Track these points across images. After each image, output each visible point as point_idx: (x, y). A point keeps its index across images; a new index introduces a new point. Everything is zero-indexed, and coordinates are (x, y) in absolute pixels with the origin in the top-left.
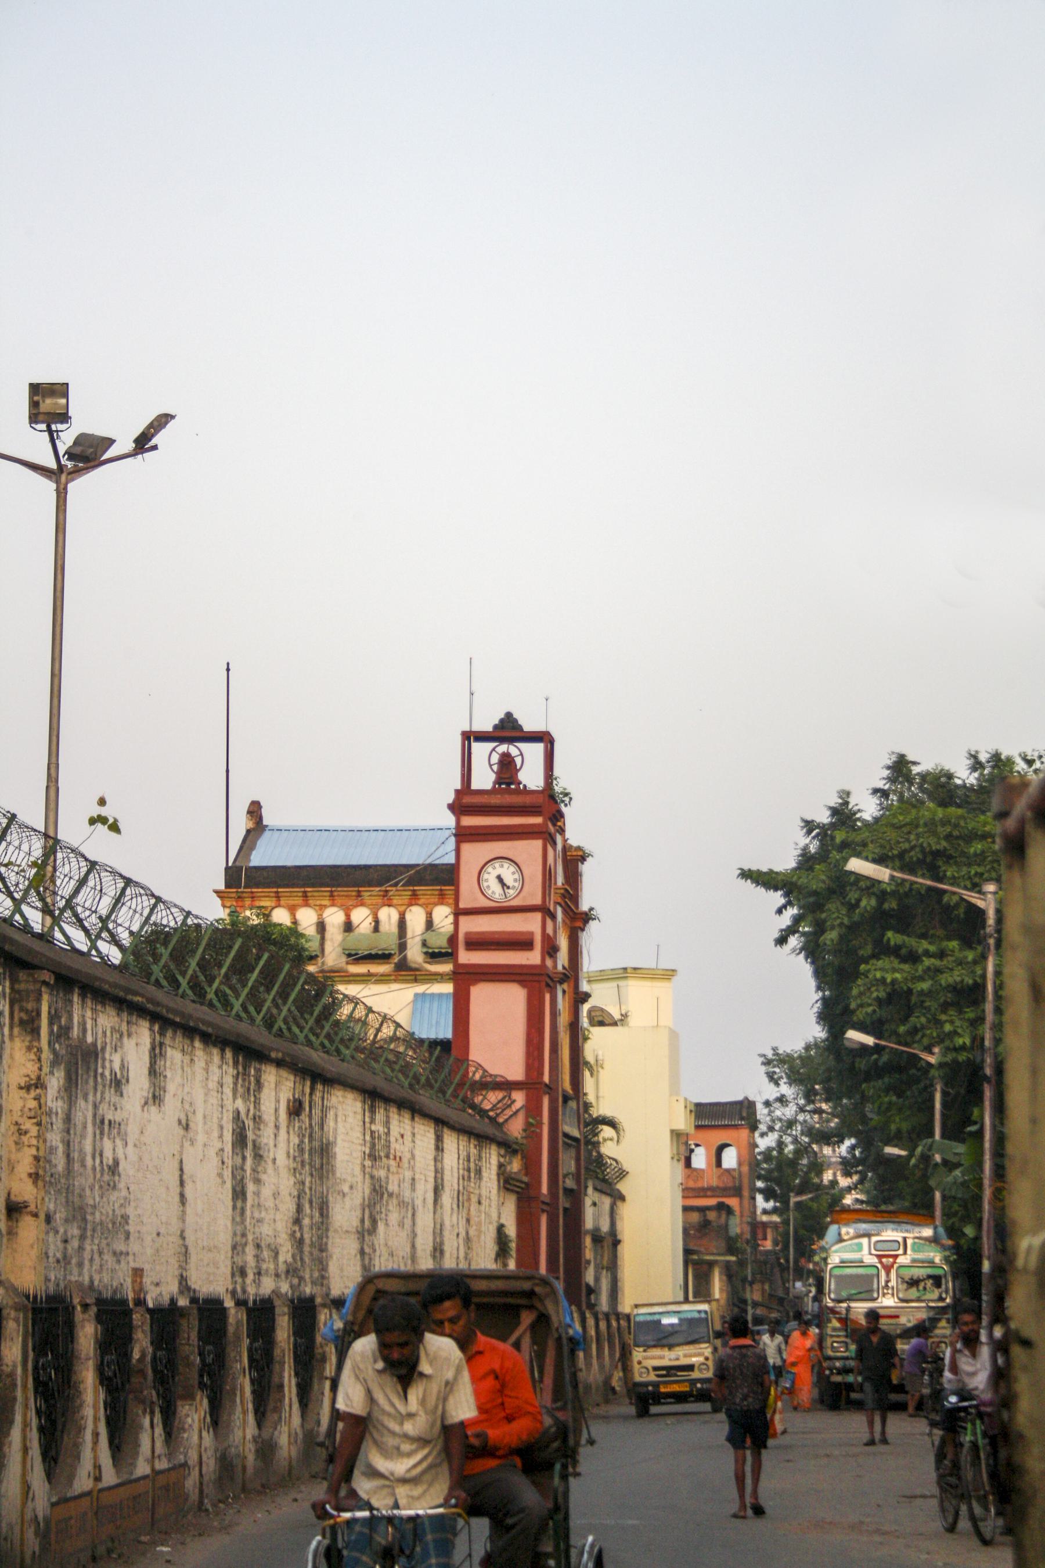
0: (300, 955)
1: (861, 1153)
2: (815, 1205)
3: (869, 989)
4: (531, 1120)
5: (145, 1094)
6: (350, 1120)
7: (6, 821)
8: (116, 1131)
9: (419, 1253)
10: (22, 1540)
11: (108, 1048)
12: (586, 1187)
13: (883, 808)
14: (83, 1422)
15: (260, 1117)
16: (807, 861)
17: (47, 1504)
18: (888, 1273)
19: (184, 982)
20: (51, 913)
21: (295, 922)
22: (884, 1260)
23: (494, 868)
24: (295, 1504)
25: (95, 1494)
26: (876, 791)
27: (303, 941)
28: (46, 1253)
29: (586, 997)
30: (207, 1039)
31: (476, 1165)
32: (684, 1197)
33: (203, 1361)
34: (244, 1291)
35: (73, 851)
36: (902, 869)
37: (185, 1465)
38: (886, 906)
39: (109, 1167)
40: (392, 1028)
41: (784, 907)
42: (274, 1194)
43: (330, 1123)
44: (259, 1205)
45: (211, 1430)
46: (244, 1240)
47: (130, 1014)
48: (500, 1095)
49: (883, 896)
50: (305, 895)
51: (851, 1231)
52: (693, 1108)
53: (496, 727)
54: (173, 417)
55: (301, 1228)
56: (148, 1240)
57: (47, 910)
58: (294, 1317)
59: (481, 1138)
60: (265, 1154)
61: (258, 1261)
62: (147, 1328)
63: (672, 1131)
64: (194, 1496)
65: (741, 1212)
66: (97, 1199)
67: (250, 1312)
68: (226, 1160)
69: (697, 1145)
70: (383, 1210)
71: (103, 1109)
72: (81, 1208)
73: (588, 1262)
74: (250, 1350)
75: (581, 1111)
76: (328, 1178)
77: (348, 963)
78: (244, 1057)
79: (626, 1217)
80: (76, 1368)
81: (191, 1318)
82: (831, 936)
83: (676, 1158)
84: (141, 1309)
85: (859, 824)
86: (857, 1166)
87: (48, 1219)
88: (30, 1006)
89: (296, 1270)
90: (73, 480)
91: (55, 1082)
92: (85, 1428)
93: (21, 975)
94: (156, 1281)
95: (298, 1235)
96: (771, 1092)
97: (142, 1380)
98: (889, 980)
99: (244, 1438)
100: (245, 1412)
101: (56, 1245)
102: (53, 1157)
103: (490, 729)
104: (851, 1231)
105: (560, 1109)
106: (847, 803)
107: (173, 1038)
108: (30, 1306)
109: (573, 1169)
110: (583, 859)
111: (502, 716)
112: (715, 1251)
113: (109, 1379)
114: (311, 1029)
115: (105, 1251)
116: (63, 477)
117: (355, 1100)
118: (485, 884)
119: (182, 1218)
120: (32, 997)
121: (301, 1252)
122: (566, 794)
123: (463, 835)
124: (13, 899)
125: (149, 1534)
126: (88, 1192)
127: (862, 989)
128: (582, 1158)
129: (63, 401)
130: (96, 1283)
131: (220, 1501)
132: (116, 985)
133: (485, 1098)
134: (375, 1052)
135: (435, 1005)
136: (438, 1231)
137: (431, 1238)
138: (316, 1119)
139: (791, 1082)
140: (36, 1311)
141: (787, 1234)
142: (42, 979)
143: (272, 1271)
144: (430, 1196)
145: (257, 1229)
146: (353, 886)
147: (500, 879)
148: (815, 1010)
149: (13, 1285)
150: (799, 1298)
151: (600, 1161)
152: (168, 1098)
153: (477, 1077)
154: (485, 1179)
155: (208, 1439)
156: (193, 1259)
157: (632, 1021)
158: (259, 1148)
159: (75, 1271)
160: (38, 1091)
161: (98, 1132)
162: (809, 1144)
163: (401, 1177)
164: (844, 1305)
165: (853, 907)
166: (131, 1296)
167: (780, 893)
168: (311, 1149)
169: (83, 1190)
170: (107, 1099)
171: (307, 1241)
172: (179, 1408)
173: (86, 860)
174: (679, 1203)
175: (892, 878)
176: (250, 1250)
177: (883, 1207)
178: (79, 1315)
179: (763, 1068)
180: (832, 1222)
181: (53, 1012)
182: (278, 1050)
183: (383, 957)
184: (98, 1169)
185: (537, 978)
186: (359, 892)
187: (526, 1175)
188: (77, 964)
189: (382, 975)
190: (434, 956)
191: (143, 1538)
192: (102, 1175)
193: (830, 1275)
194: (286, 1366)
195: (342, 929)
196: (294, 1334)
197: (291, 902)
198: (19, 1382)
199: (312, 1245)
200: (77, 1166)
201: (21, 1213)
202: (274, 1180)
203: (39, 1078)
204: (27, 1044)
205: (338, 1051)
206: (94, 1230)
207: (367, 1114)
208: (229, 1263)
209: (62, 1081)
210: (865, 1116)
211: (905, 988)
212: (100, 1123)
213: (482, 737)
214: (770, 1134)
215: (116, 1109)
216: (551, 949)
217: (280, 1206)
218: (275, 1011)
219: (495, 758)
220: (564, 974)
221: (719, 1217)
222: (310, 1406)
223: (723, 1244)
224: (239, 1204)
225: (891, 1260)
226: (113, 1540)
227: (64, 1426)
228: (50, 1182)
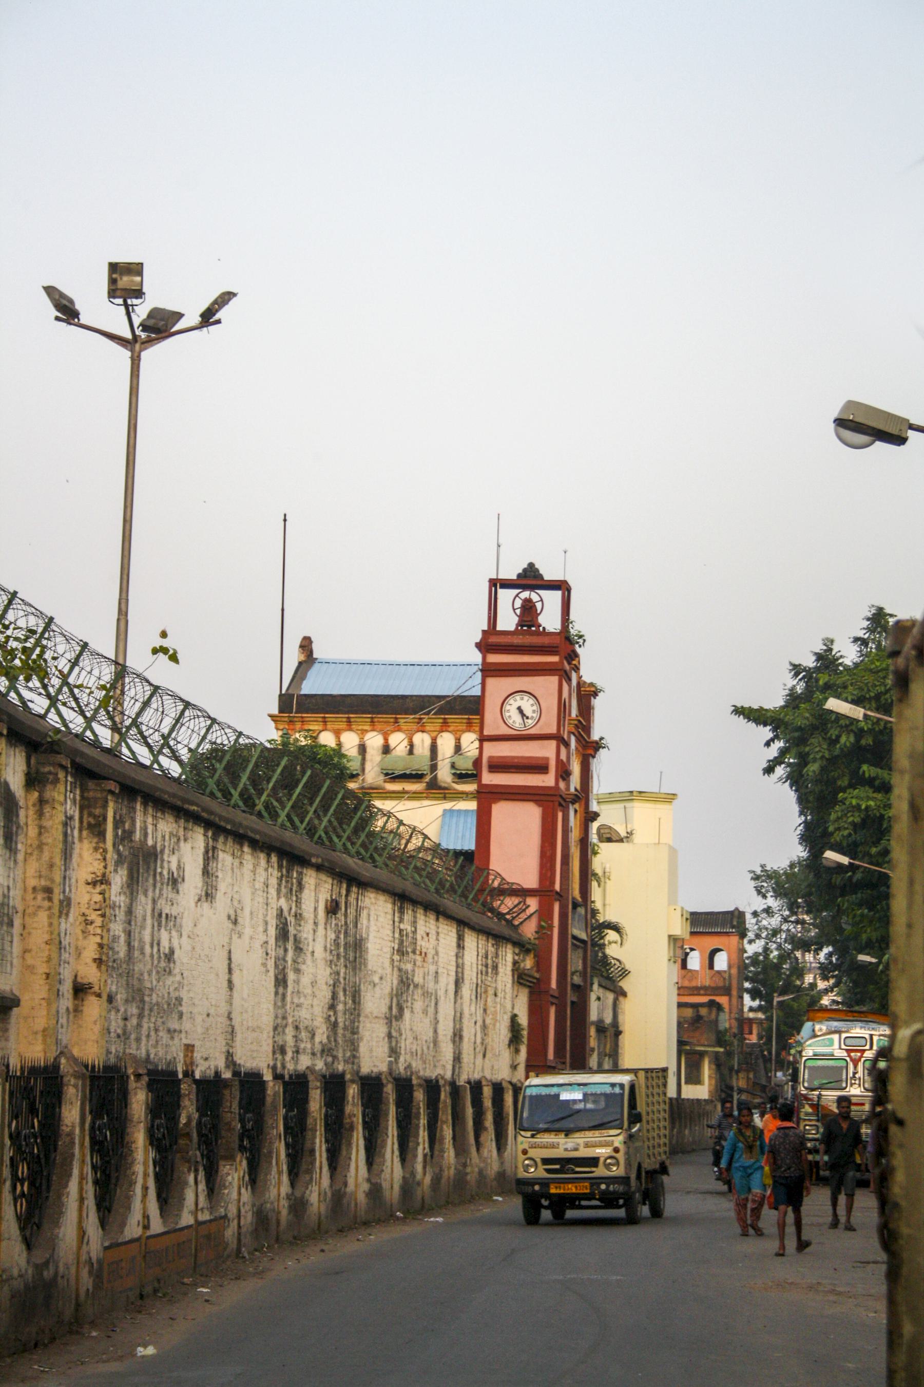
0: (342, 773)
1: (837, 959)
2: (795, 1005)
3: (846, 815)
4: (543, 924)
5: (199, 891)
6: (381, 919)
7: (79, 648)
8: (172, 923)
9: (441, 1037)
10: (77, 1279)
11: (167, 851)
12: (592, 984)
13: (862, 655)
14: (134, 1177)
15: (300, 915)
16: (793, 700)
17: (99, 1248)
18: (855, 1066)
19: (236, 794)
20: (120, 733)
21: (339, 744)
22: (852, 1054)
23: (515, 701)
24: (322, 1254)
25: (143, 1241)
26: (856, 640)
27: (345, 761)
28: (108, 1029)
29: (595, 816)
30: (256, 845)
31: (494, 962)
32: (679, 995)
33: (243, 1127)
34: (284, 1067)
35: (138, 676)
36: (877, 710)
37: (225, 1217)
38: (863, 742)
39: (166, 955)
40: (421, 840)
41: (772, 740)
42: (312, 983)
43: (363, 921)
44: (298, 992)
45: (249, 1187)
46: (285, 1022)
47: (187, 821)
48: (516, 900)
49: (860, 734)
50: (349, 721)
51: (824, 1028)
53: (519, 576)
54: (234, 295)
55: (335, 1013)
56: (199, 1019)
57: (115, 728)
59: (499, 938)
60: (305, 948)
61: (296, 1041)
62: (193, 1096)
63: (670, 936)
64: (233, 1245)
65: (730, 1009)
66: (155, 983)
67: (286, 1084)
68: (269, 951)
69: (692, 949)
70: (409, 999)
71: (161, 903)
72: (139, 990)
73: (593, 1050)
74: (285, 1118)
75: (589, 916)
76: (360, 969)
77: (385, 782)
78: (288, 861)
79: (627, 1012)
80: (128, 1130)
81: (233, 1089)
82: (813, 768)
83: (673, 960)
84: (189, 1080)
85: (841, 668)
86: (834, 971)
87: (110, 999)
88: (97, 812)
89: (330, 1050)
90: (145, 349)
91: (118, 879)
92: (135, 1183)
93: (90, 784)
94: (205, 1056)
95: (333, 1019)
96: (759, 904)
97: (188, 1142)
98: (863, 807)
99: (279, 1195)
100: (280, 1173)
101: (116, 1022)
102: (116, 944)
103: (515, 578)
104: (824, 1028)
105: (570, 914)
106: (831, 650)
107: (225, 843)
108: (88, 1074)
109: (580, 967)
110: (595, 694)
111: (525, 566)
112: (706, 1043)
113: (158, 1140)
114: (349, 839)
115: (161, 1028)
116: (137, 346)
117: (386, 901)
119: (230, 1002)
120: (100, 803)
121: (336, 1034)
122: (581, 637)
123: (488, 671)
124: (85, 717)
125: (192, 1277)
126: (146, 976)
127: (840, 814)
128: (589, 958)
129: (138, 279)
130: (152, 1056)
131: (256, 1250)
132: (174, 795)
133: (502, 903)
134: (405, 860)
135: (462, 819)
136: (458, 1018)
137: (451, 1024)
138: (351, 917)
139: (778, 894)
140: (93, 1078)
141: (771, 1028)
142: (108, 788)
144: (452, 987)
145: (296, 1013)
147: (520, 709)
148: (798, 832)
149: (73, 1056)
150: (780, 1086)
151: (605, 961)
152: (219, 895)
153: (496, 884)
154: (500, 974)
155: (246, 1195)
156: (239, 1038)
157: (637, 838)
158: (300, 942)
159: (134, 1045)
160: (103, 886)
161: (156, 924)
162: (793, 951)
163: (426, 970)
164: (817, 1093)
165: (834, 742)
166: (180, 1069)
167: (769, 728)
168: (346, 944)
169: (142, 975)
170: (165, 896)
171: (341, 1025)
172: (221, 1168)
173: (151, 684)
174: (675, 999)
175: (866, 716)
176: (290, 1031)
177: (857, 1008)
178: (132, 1083)
179: (753, 884)
180: (808, 1020)
181: (118, 817)
182: (318, 857)
183: (416, 777)
184: (156, 956)
185: (549, 798)
186: (396, 718)
187: (538, 971)
188: (141, 776)
189: (414, 793)
190: (461, 777)
191: (186, 1280)
192: (159, 962)
193: (805, 1067)
194: (318, 1133)
195: (381, 751)
196: (325, 1105)
197: (336, 727)
198: (77, 1141)
199: (345, 1028)
200: (137, 953)
201: (86, 993)
202: (311, 970)
203: (104, 875)
204: (94, 845)
205: (372, 857)
206: (151, 1010)
207: (397, 915)
208: (270, 1041)
209: (125, 879)
210: (841, 928)
211: (878, 815)
212: (158, 916)
213: (507, 584)
214: (757, 941)
215: (172, 904)
216: (564, 773)
217: (317, 993)
218: (316, 822)
219: (518, 603)
221: (710, 1013)
222: (339, 1169)
223: (713, 1037)
224: (281, 990)
225: (859, 1054)
226: (159, 1281)
227: (118, 1179)
228: (113, 967)
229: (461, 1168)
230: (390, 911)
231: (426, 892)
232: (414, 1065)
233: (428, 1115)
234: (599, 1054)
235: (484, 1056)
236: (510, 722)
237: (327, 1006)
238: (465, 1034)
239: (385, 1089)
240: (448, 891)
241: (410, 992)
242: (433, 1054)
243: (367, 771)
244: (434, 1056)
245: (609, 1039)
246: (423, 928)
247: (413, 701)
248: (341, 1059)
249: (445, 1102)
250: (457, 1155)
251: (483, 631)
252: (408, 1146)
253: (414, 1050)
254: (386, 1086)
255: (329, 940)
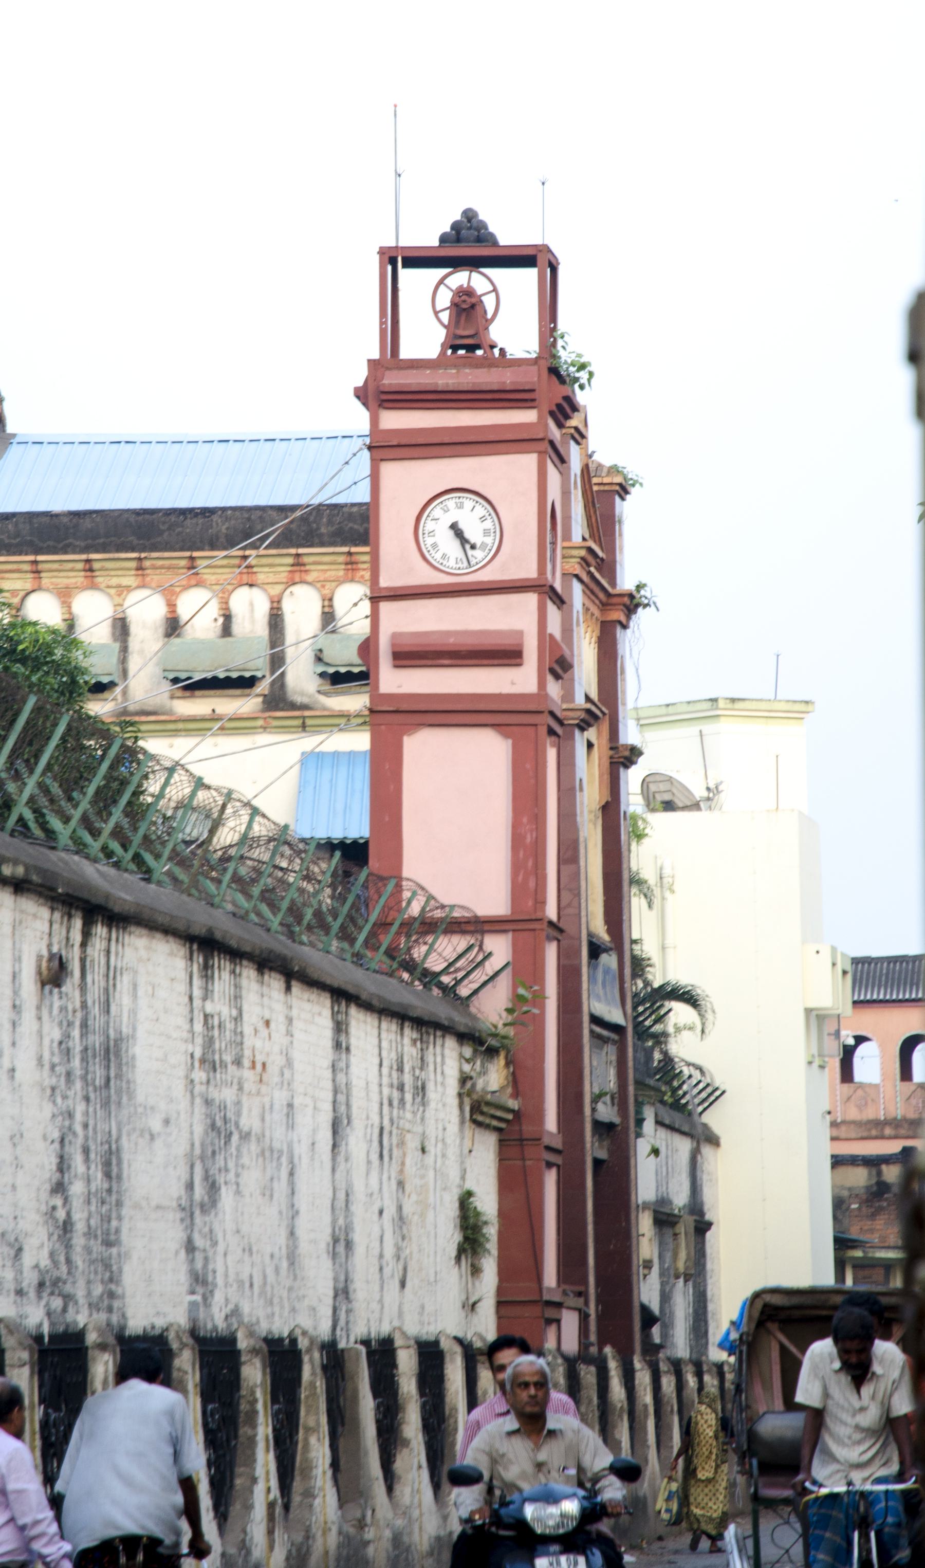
0: (74, 682)
4: (521, 991)
9: (304, 1247)
12: (640, 1122)
21: (71, 624)
23: (446, 511)
32: (833, 1139)
40: (245, 819)
42: (12, 1138)
43: (122, 999)
48: (460, 943)
50: (89, 568)
52: (849, 968)
53: (444, 239)
55: (66, 1200)
58: (41, 1373)
63: (808, 1011)
70: (231, 1165)
73: (648, 1265)
75: (628, 971)
76: (119, 1103)
77: (172, 697)
89: (56, 1282)
103: (436, 243)
105: (584, 969)
110: (623, 490)
111: (458, 217)
114: (85, 820)
117: (171, 954)
118: (429, 541)
121: (68, 1246)
122: (582, 367)
128: (630, 1064)
135: (343, 770)
137: (327, 1219)
143: (10, 1286)
144: (325, 1136)
146: (182, 549)
147: (457, 530)
154: (433, 1105)
163: (267, 1100)
171: (80, 1227)
174: (826, 1150)
182: (16, 862)
183: (246, 683)
186: (192, 558)
195: (161, 631)
199: (90, 1233)
207: (197, 982)
219: (445, 298)
220: (588, 711)
229: (352, 1531)
230: (182, 975)
231: (261, 932)
232: (246, 1309)
233: (275, 1415)
234: (662, 1274)
235: (403, 1284)
236: (435, 557)
237: (47, 1187)
238: (358, 1237)
239: (177, 1362)
240: (309, 928)
241: (233, 1150)
242: (288, 1283)
243: (131, 673)
244: (290, 1289)
245: (682, 1238)
246: (257, 1010)
247: (227, 519)
248: (82, 1301)
249: (312, 1385)
250: (342, 1502)
251: (371, 362)
252: (232, 1486)
253: (245, 1277)
254: (179, 1355)
255: (46, 1042)
